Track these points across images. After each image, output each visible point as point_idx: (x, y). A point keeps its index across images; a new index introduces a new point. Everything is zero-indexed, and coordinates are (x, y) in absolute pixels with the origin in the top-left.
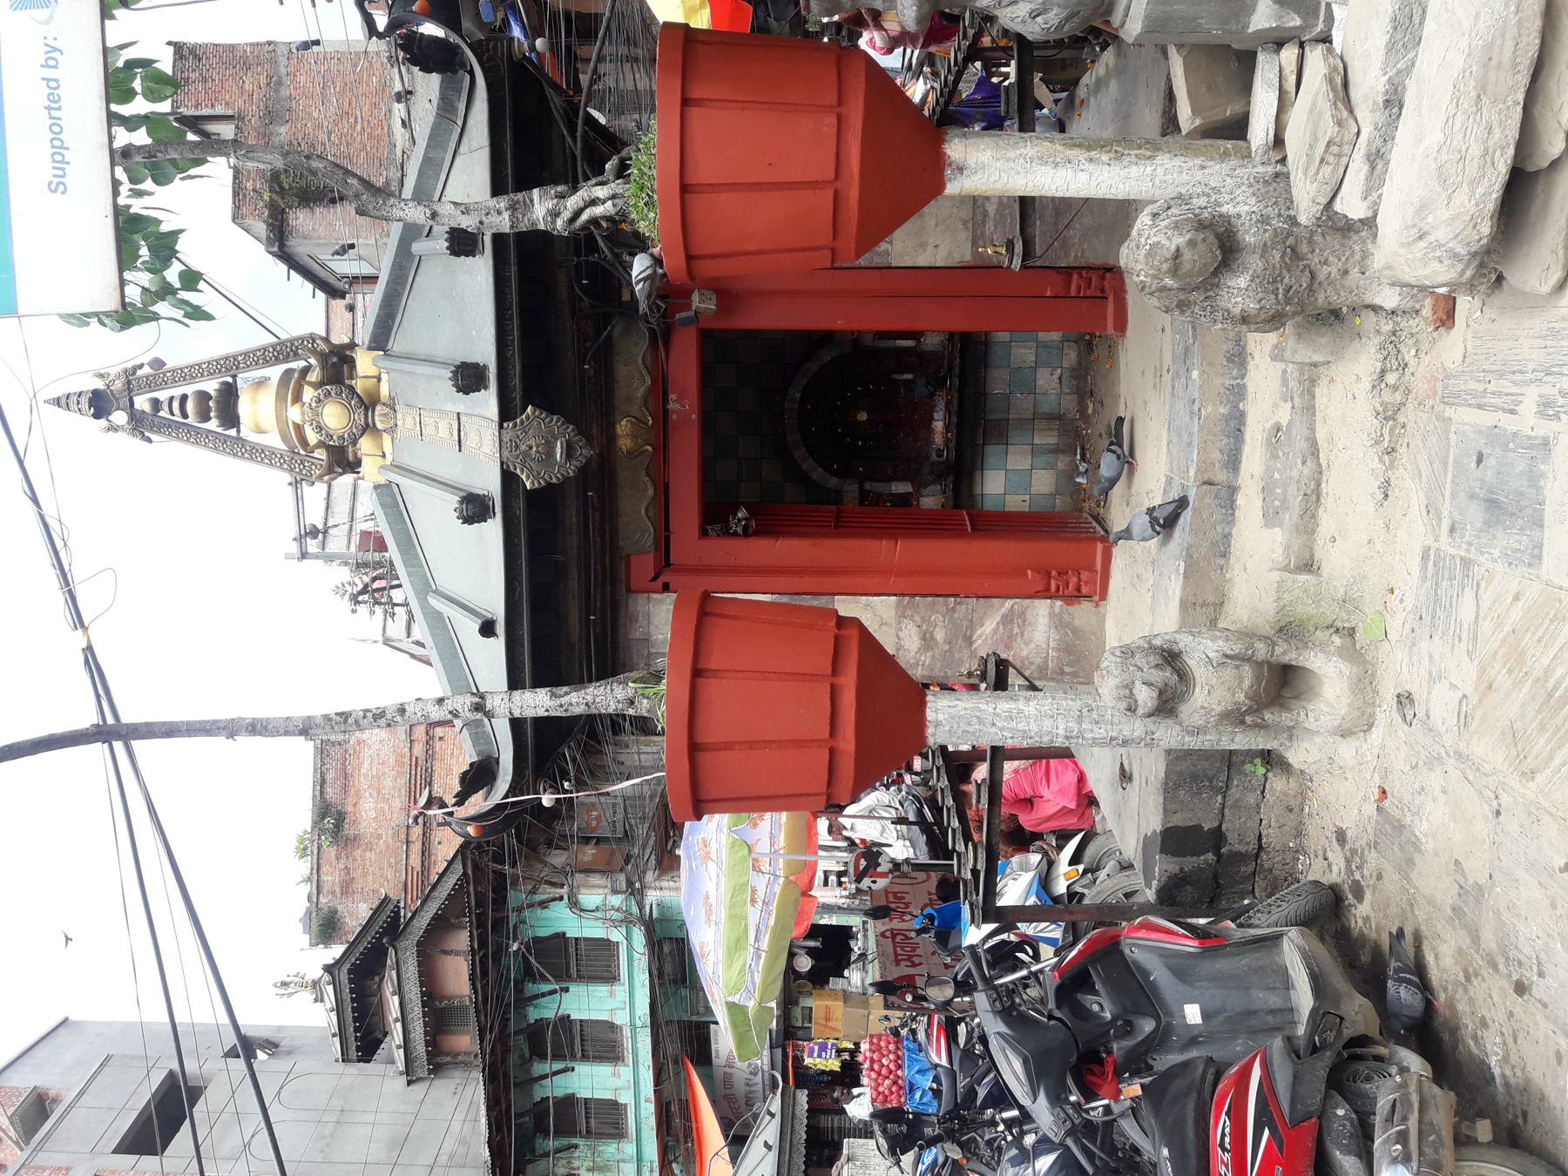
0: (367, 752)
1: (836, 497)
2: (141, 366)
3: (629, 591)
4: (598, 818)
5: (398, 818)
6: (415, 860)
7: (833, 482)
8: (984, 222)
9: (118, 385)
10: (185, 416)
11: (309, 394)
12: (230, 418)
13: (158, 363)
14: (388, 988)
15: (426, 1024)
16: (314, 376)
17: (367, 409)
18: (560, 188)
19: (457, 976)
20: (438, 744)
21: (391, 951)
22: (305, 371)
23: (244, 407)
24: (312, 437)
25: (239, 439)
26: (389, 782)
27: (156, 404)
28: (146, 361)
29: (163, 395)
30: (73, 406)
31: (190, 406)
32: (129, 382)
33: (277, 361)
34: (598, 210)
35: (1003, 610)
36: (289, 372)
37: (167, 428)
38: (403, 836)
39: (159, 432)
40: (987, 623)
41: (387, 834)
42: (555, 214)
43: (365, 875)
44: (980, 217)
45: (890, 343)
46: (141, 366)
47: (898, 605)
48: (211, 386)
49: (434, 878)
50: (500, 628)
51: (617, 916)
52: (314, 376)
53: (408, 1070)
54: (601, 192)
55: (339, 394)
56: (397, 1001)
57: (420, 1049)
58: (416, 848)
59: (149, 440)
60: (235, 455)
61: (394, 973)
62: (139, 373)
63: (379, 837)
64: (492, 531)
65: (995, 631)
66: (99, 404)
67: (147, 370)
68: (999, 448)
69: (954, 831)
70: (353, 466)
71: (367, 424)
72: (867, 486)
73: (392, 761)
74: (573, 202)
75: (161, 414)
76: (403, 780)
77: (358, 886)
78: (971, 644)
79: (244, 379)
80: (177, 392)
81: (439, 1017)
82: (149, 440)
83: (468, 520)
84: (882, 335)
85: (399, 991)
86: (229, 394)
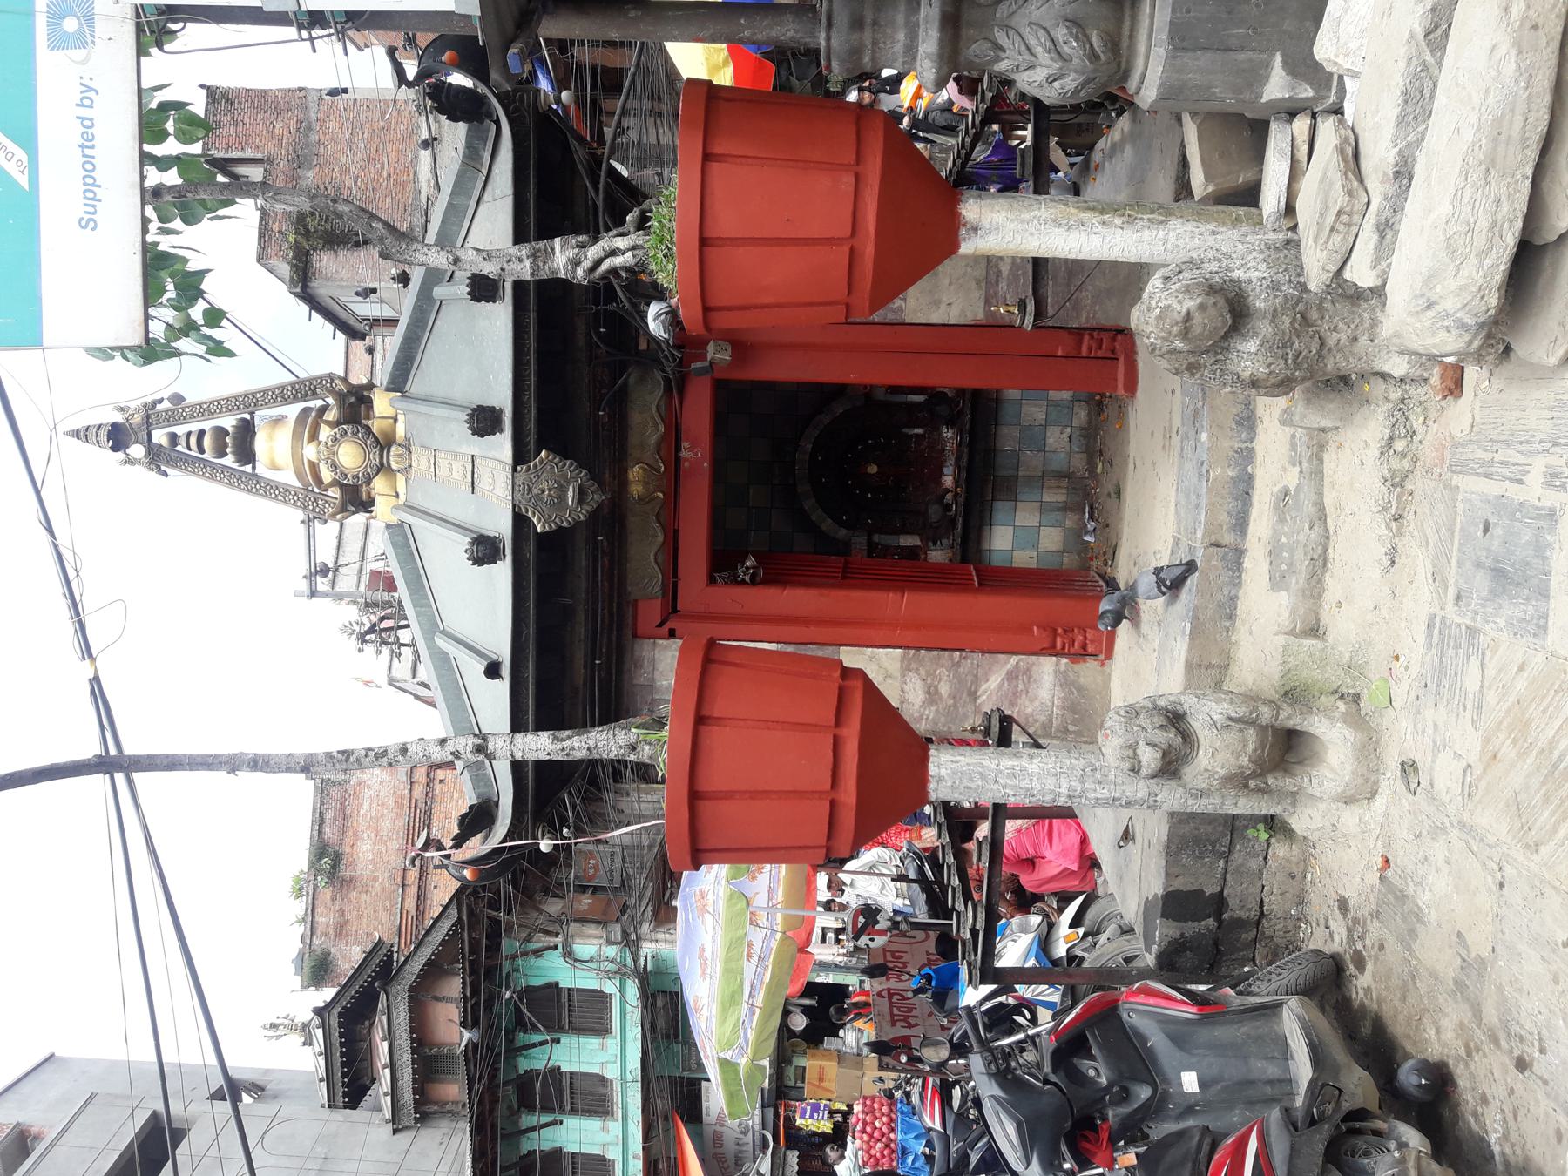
1: (844, 549)
2: (161, 401)
3: (635, 636)
4: (596, 867)
5: (396, 861)
6: (411, 904)
7: (842, 533)
8: (997, 282)
9: (137, 419)
10: (202, 451)
11: (325, 432)
12: (246, 454)
13: (177, 399)
14: (378, 1034)
15: (414, 1072)
16: (331, 416)
17: (382, 449)
18: (581, 238)
19: (452, 1030)
20: (438, 787)
21: (383, 996)
22: (323, 410)
23: (261, 444)
24: (327, 475)
25: (255, 476)
26: (387, 824)
27: (174, 438)
28: (166, 396)
29: (180, 430)
30: (92, 438)
31: (207, 442)
32: (148, 417)
33: (295, 399)
34: (618, 261)
36: (306, 411)
37: (184, 462)
38: (399, 880)
39: (175, 466)
40: (992, 679)
41: (383, 877)
42: (576, 263)
43: (359, 917)
44: (993, 277)
46: (161, 401)
47: (903, 658)
48: (229, 422)
49: (428, 923)
50: (506, 671)
51: (611, 967)
52: (331, 416)
53: (395, 1118)
54: (621, 243)
56: (386, 1047)
57: (408, 1097)
58: (412, 891)
59: (166, 474)
60: (250, 491)
61: (384, 1018)
62: (159, 407)
63: (375, 879)
64: (502, 572)
65: (1001, 686)
66: (118, 437)
67: (166, 405)
69: (954, 889)
70: (366, 505)
71: (382, 464)
72: (876, 538)
73: (391, 803)
74: (594, 252)
75: (179, 448)
76: (402, 822)
77: (351, 928)
78: (975, 699)
79: (262, 416)
80: (195, 427)
81: (428, 1063)
82: (166, 474)
83: (478, 561)
84: (895, 389)
85: (389, 1037)
86: (246, 430)
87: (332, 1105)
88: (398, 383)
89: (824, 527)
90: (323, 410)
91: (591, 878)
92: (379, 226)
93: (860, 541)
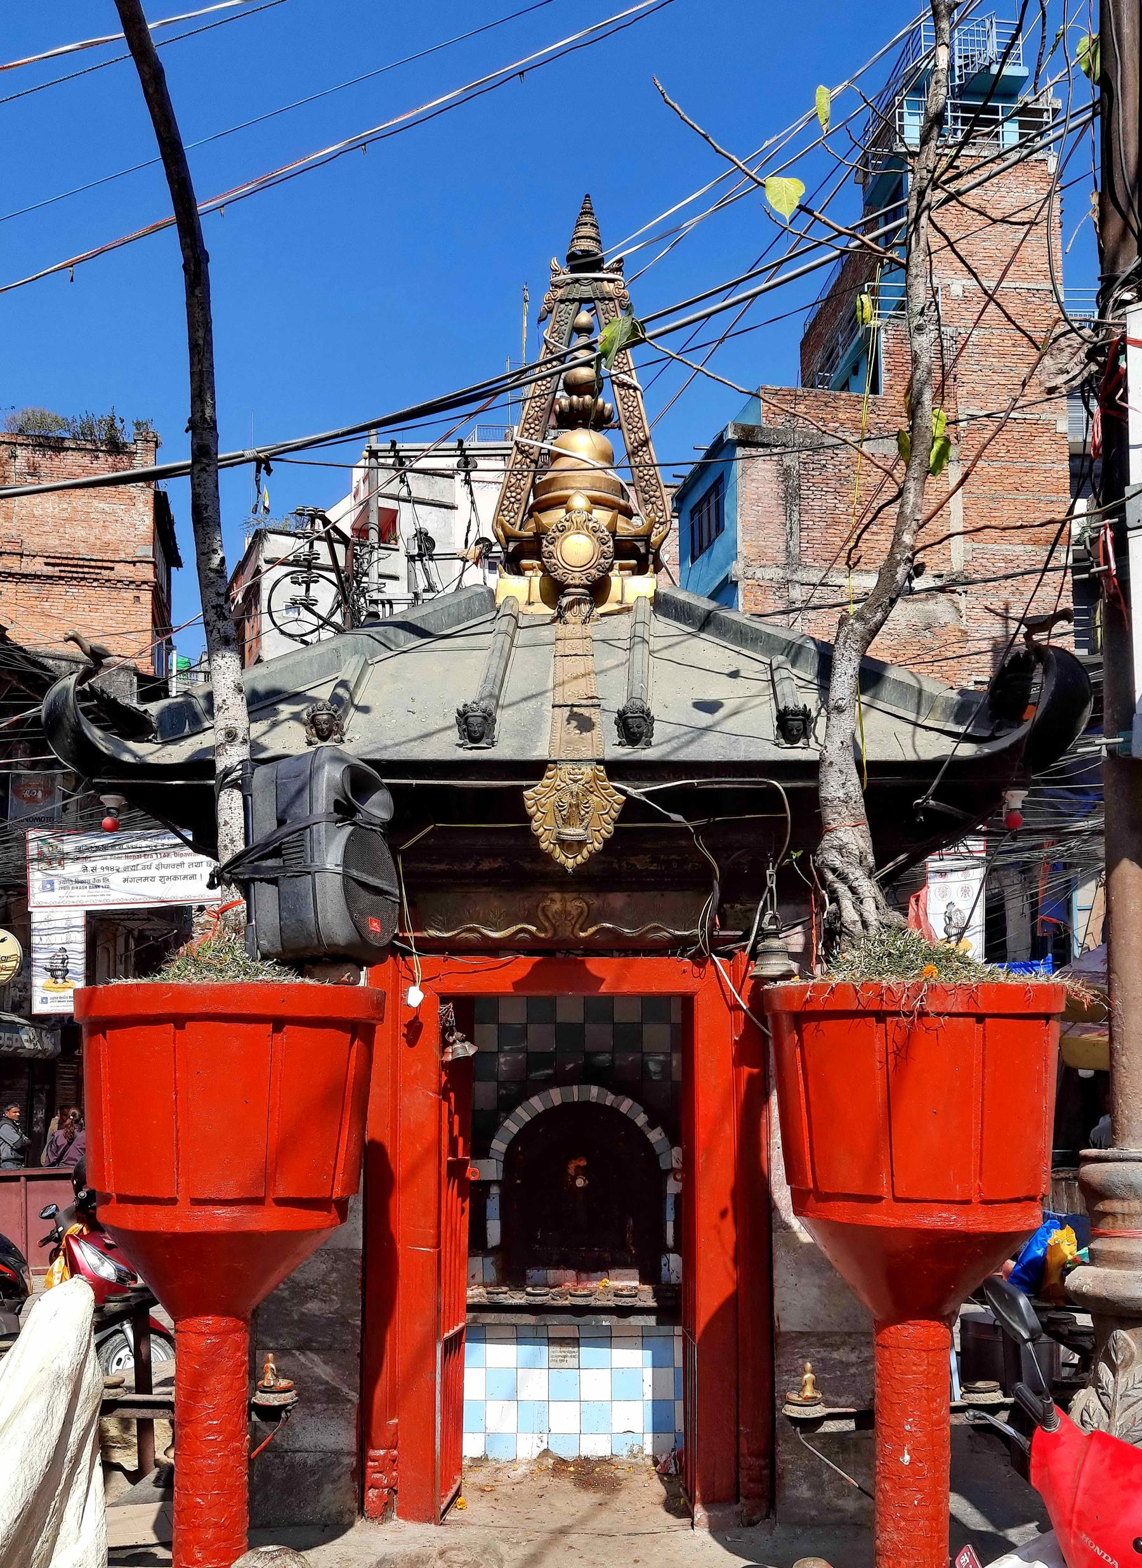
0: (119, 509)
1: (481, 1151)
5: (32, 543)
7: (499, 1145)
8: (825, 1345)
11: (602, 516)
16: (623, 525)
18: (871, 859)
20: (129, 595)
22: (628, 513)
24: (555, 516)
26: (81, 533)
34: (847, 902)
35: (345, 1390)
40: (328, 1369)
42: (840, 849)
44: (831, 1340)
45: (670, 1215)
47: (350, 1251)
52: (623, 525)
54: (869, 907)
55: (603, 555)
64: (447, 747)
65: (318, 1380)
68: (492, 1274)
70: (513, 565)
72: (495, 1190)
73: (107, 538)
74: (857, 874)
76: (84, 552)
78: (298, 1349)
83: (463, 716)
87: (110, 1549)
88: (661, 604)
89: (508, 1123)
90: (628, 513)
91: (17, 792)
92: (879, 616)
93: (489, 1170)
